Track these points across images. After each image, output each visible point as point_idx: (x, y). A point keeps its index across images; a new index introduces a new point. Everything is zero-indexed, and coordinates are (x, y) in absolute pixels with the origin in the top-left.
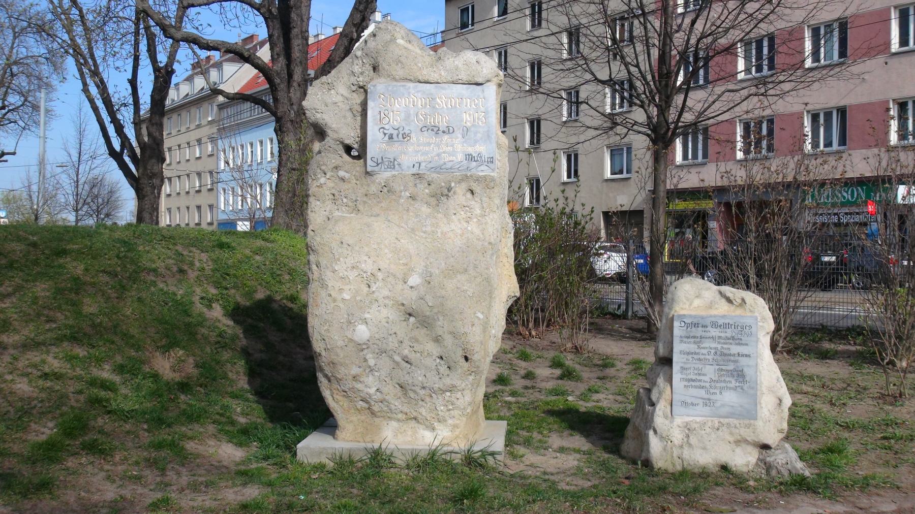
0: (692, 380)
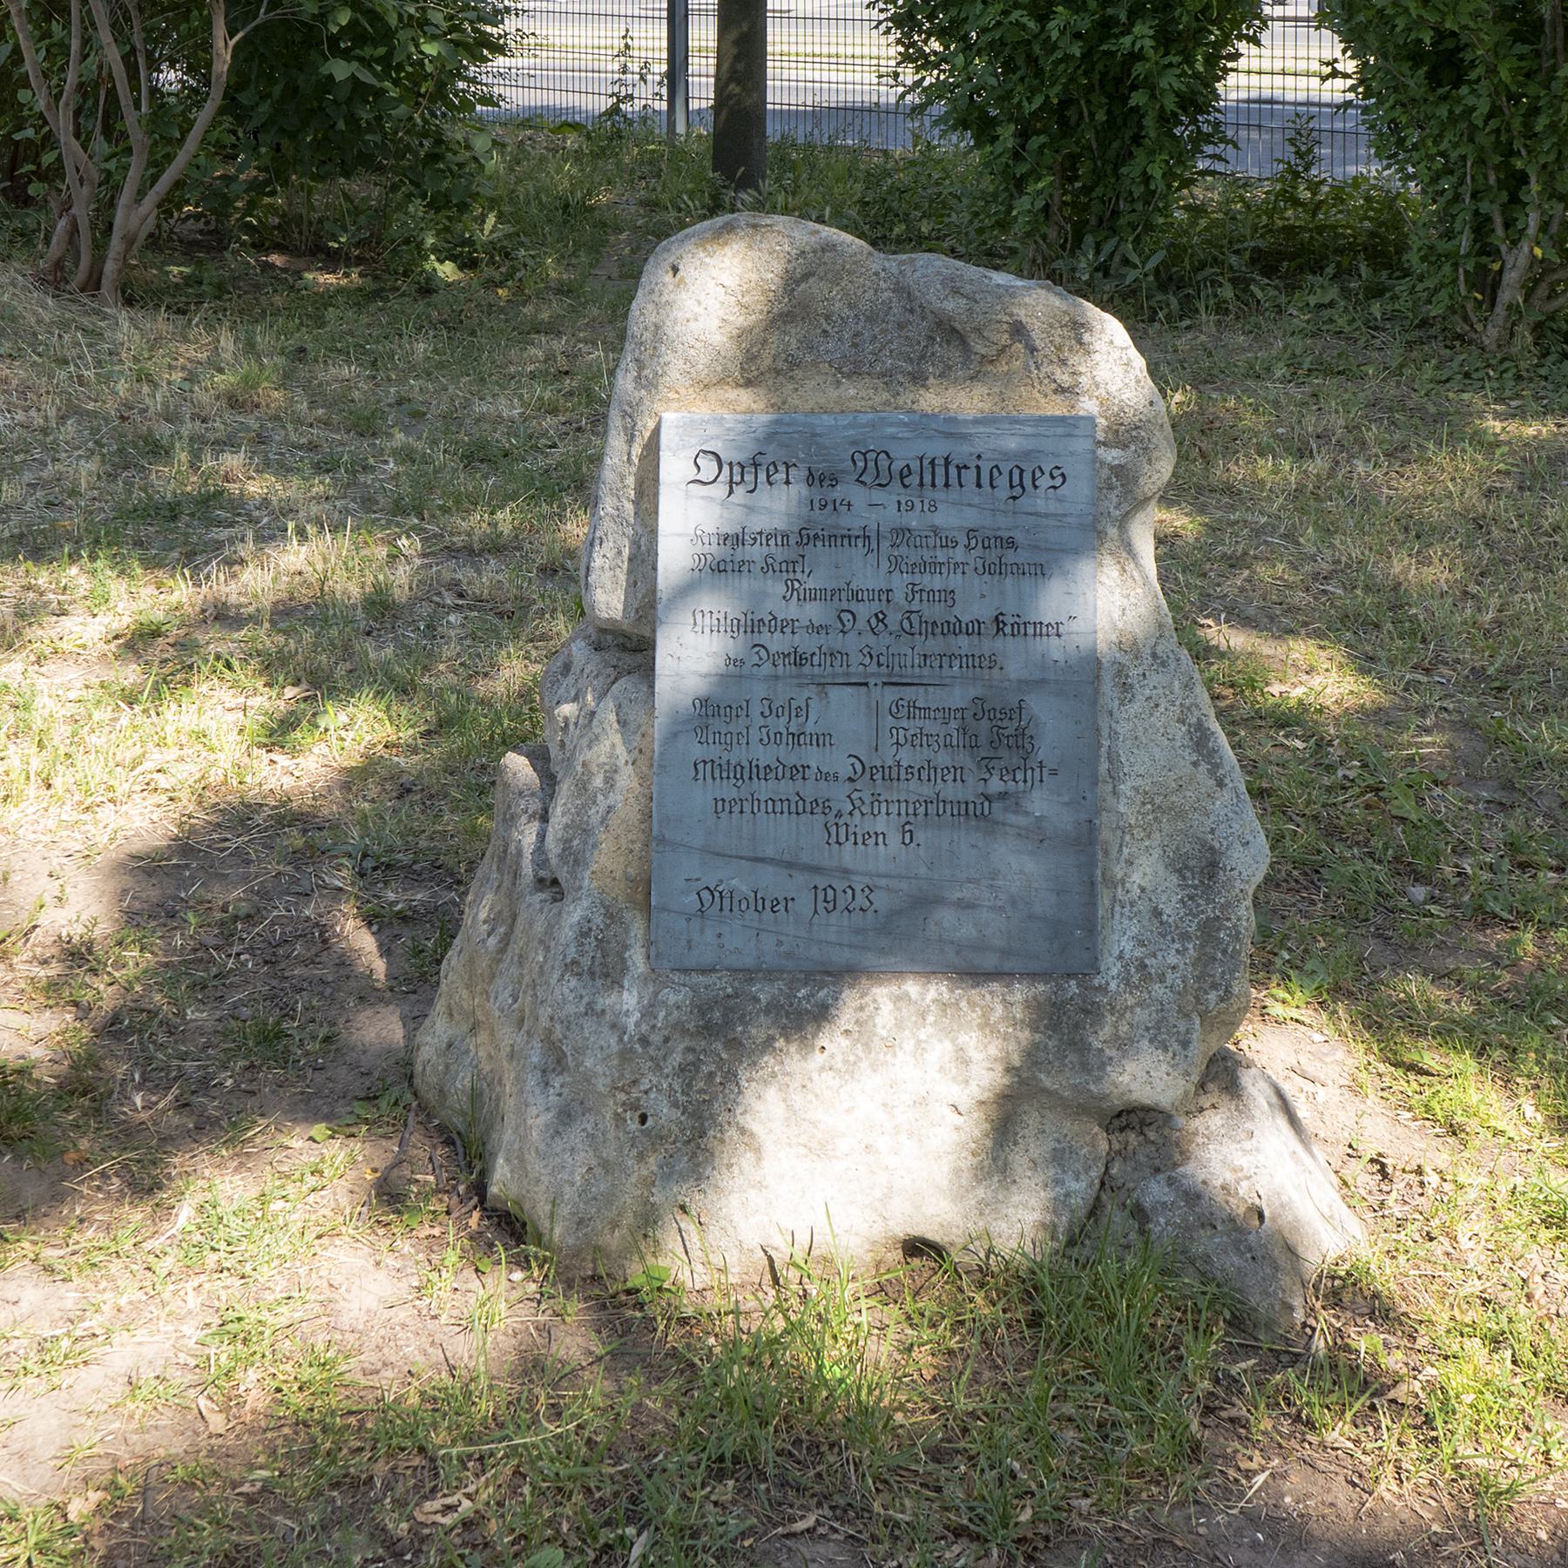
0: (759, 772)
